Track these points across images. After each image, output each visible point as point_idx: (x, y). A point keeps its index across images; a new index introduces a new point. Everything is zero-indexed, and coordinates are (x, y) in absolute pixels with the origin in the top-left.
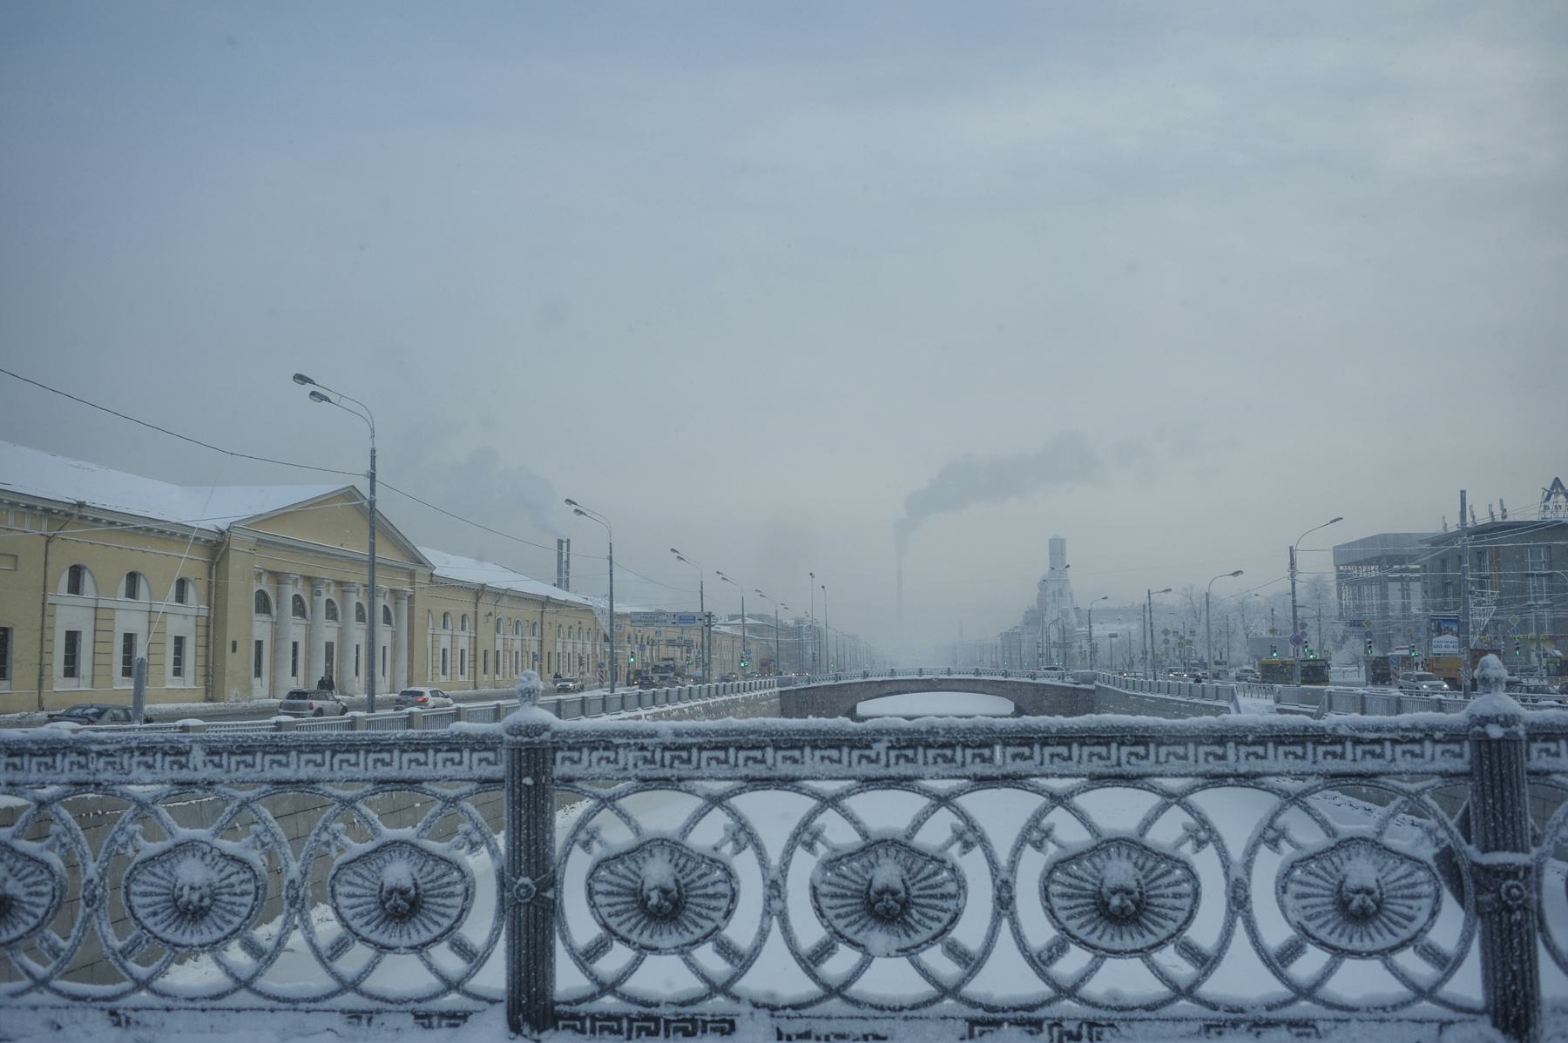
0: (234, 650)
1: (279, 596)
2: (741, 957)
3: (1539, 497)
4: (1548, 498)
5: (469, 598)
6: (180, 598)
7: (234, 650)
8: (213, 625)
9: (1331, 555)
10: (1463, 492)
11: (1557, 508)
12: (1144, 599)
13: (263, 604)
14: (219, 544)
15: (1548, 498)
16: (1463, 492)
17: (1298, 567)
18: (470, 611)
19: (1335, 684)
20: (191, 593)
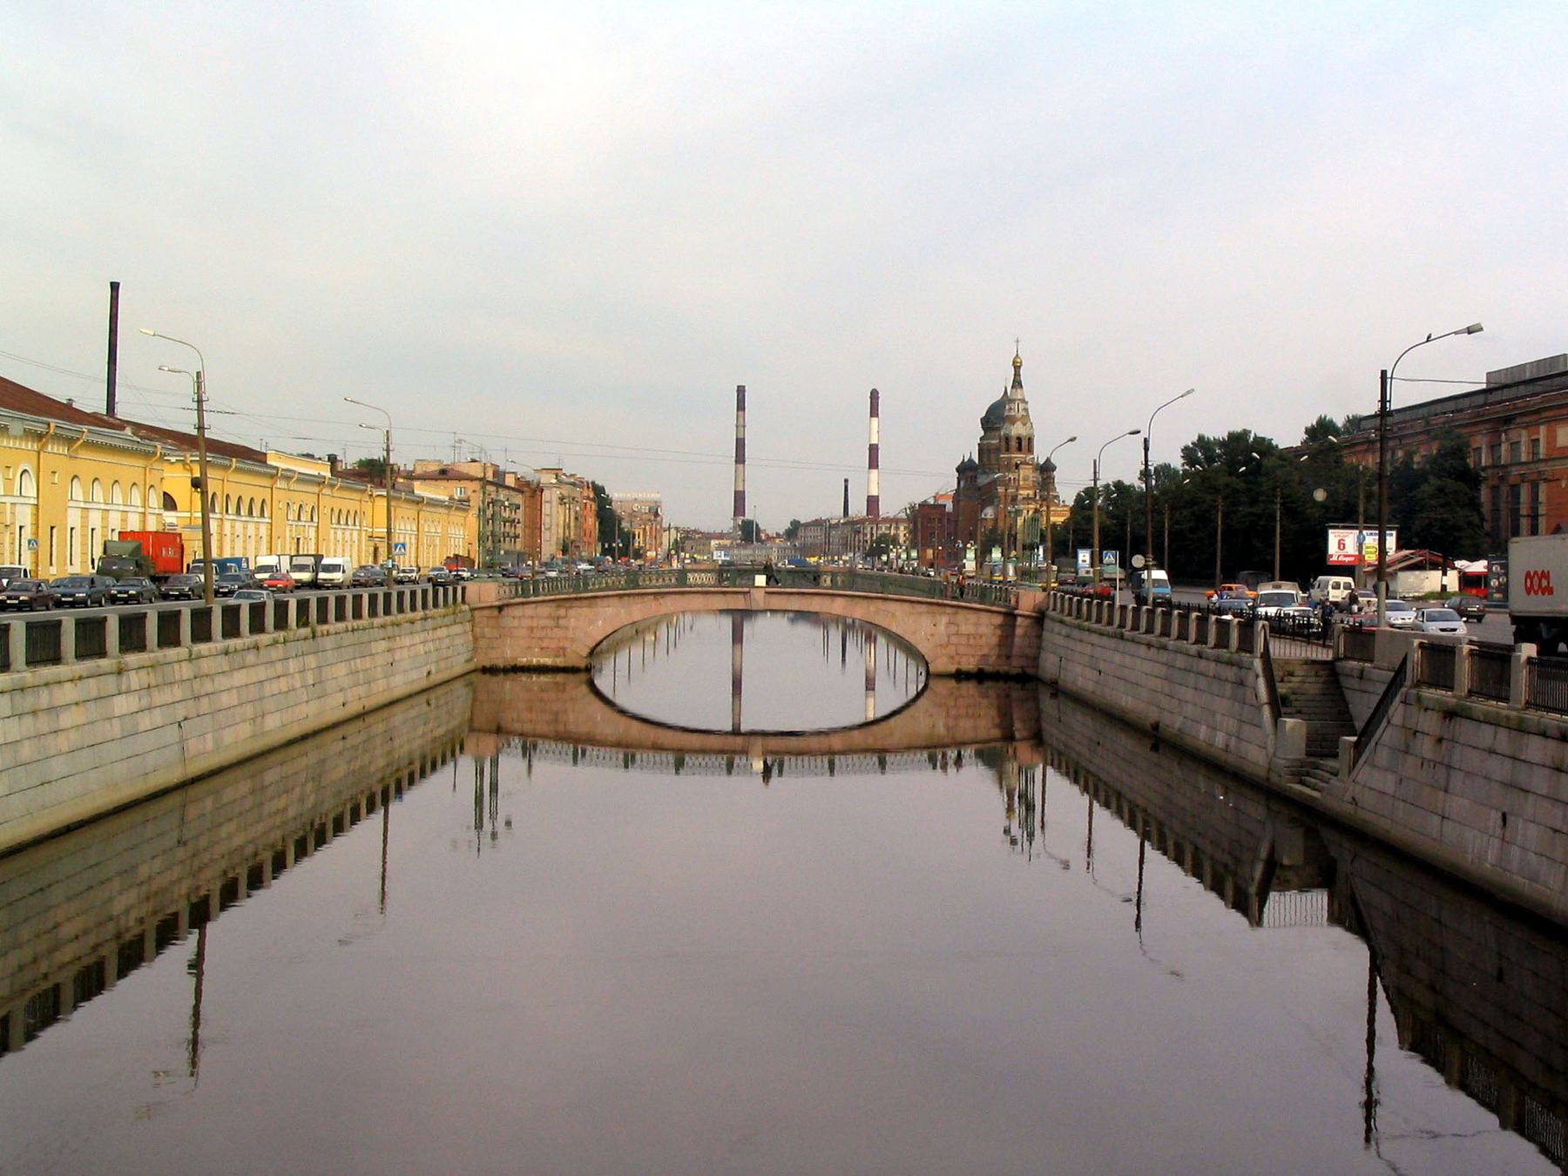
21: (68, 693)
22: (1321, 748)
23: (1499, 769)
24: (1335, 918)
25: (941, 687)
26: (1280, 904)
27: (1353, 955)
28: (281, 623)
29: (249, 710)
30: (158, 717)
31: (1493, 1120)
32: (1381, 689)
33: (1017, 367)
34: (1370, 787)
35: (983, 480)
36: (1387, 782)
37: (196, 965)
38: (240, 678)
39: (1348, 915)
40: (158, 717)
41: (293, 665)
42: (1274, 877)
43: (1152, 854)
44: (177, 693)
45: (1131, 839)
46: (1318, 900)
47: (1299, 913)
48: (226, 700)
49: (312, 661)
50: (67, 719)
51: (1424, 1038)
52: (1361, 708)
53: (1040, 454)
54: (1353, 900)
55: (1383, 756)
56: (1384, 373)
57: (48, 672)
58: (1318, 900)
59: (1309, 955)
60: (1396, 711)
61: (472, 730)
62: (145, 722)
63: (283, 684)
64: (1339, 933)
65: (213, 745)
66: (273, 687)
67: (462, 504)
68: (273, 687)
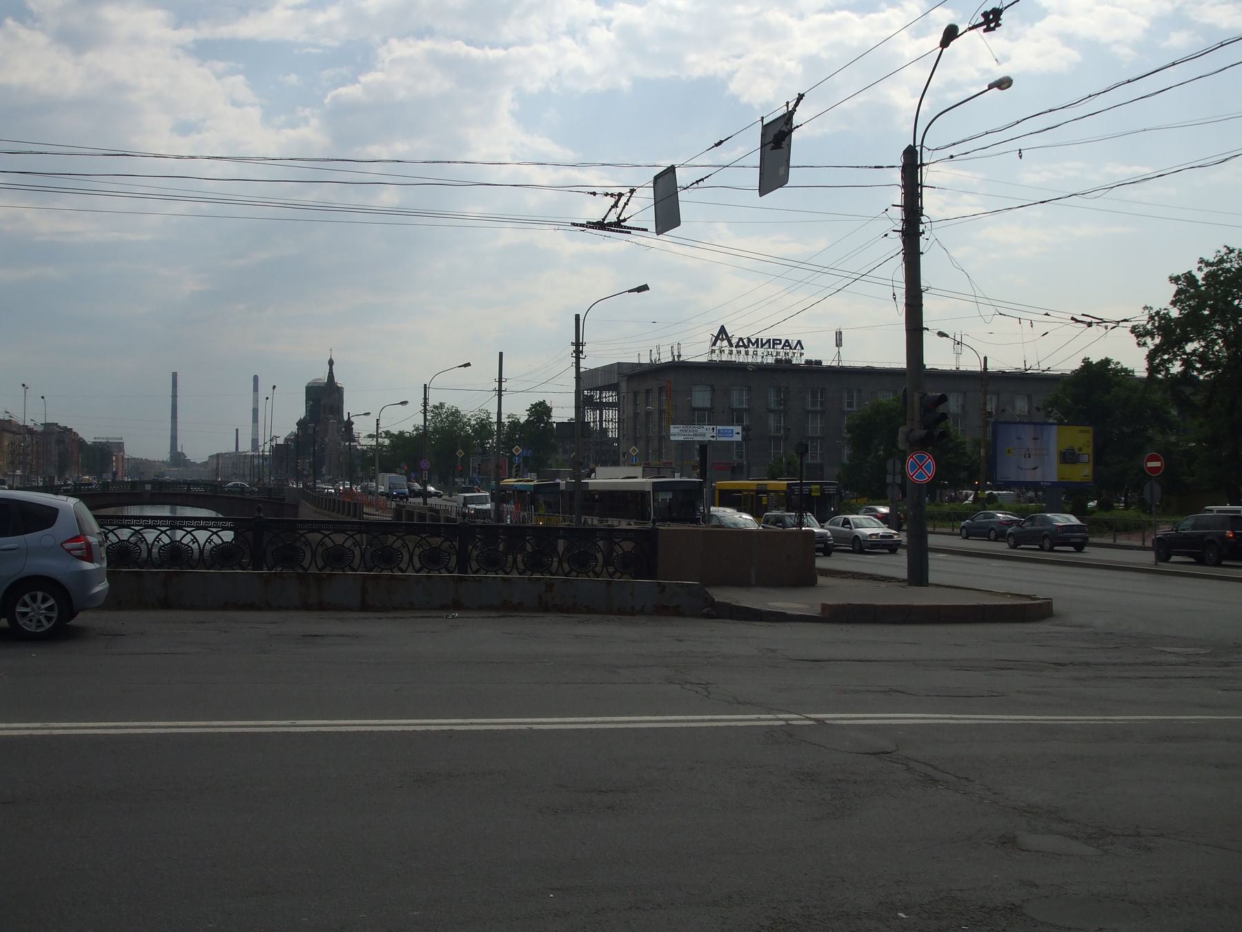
3: (708, 339)
4: (714, 344)
11: (722, 351)
15: (714, 344)
33: (331, 363)
56: (577, 317)
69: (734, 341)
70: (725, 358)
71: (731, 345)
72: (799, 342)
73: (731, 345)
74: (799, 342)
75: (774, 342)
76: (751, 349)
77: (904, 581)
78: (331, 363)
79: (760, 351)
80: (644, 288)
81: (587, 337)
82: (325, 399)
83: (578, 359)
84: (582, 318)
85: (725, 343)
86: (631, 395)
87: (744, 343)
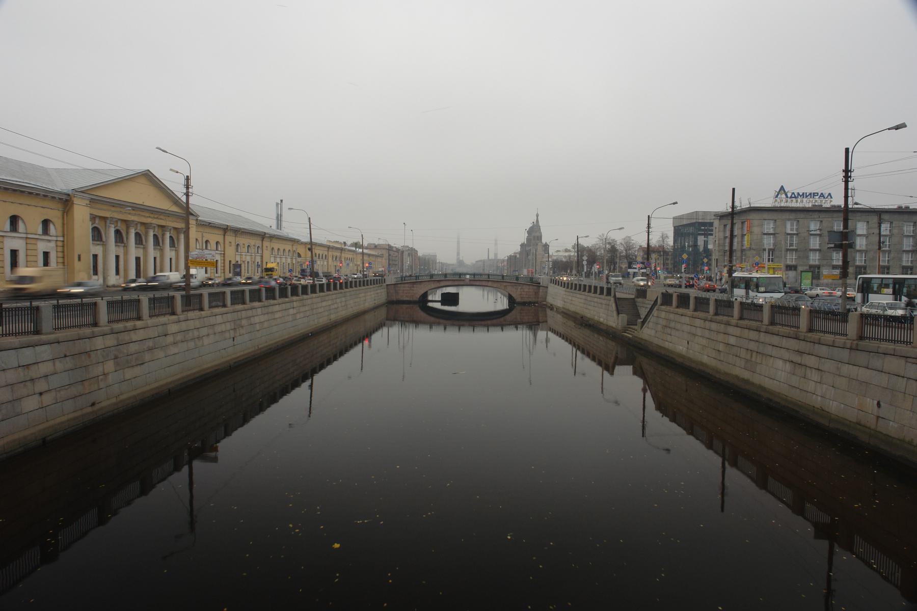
0: (79, 259)
1: (127, 233)
2: (813, 272)
3: (773, 194)
4: (777, 196)
5: (221, 232)
6: (46, 231)
7: (79, 259)
8: (66, 246)
9: (671, 221)
10: (734, 189)
11: (781, 201)
12: (575, 241)
13: (97, 235)
14: (67, 200)
15: (777, 196)
16: (734, 189)
17: (652, 226)
18: (221, 241)
19: (47, 334)
20: (52, 229)
21: (277, 308)
22: (631, 323)
23: (687, 328)
24: (635, 373)
25: (518, 308)
26: (619, 369)
27: (639, 382)
28: (335, 288)
29: (326, 313)
30: (302, 315)
31: (684, 432)
32: (650, 306)
33: (537, 216)
34: (648, 333)
35: (528, 249)
36: (653, 333)
37: (311, 386)
38: (324, 304)
39: (639, 372)
40: (302, 315)
41: (338, 301)
42: (619, 362)
43: (605, 372)
44: (307, 308)
45: (600, 369)
46: (630, 368)
47: (625, 373)
48: (320, 310)
49: (343, 299)
50: (277, 315)
51: (661, 407)
52: (643, 312)
53: (544, 241)
54: (641, 368)
55: (651, 325)
56: (847, 150)
57: (272, 302)
58: (630, 368)
59: (626, 383)
60: (655, 312)
61: (387, 319)
62: (298, 316)
63: (336, 306)
64: (635, 377)
65: (322, 320)
66: (333, 307)
67: (381, 256)
68: (333, 307)
69: (789, 195)
70: (783, 205)
71: (787, 197)
72: (830, 194)
73: (787, 197)
74: (830, 194)
75: (813, 195)
76: (799, 200)
77: (313, 267)
78: (537, 216)
79: (805, 200)
80: (903, 126)
81: (854, 165)
82: (534, 233)
83: (846, 182)
84: (850, 150)
85: (784, 196)
86: (722, 226)
87: (795, 196)
